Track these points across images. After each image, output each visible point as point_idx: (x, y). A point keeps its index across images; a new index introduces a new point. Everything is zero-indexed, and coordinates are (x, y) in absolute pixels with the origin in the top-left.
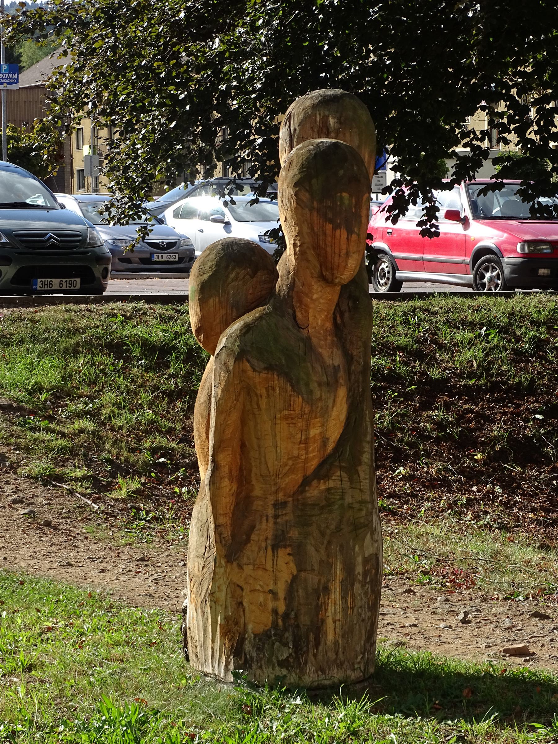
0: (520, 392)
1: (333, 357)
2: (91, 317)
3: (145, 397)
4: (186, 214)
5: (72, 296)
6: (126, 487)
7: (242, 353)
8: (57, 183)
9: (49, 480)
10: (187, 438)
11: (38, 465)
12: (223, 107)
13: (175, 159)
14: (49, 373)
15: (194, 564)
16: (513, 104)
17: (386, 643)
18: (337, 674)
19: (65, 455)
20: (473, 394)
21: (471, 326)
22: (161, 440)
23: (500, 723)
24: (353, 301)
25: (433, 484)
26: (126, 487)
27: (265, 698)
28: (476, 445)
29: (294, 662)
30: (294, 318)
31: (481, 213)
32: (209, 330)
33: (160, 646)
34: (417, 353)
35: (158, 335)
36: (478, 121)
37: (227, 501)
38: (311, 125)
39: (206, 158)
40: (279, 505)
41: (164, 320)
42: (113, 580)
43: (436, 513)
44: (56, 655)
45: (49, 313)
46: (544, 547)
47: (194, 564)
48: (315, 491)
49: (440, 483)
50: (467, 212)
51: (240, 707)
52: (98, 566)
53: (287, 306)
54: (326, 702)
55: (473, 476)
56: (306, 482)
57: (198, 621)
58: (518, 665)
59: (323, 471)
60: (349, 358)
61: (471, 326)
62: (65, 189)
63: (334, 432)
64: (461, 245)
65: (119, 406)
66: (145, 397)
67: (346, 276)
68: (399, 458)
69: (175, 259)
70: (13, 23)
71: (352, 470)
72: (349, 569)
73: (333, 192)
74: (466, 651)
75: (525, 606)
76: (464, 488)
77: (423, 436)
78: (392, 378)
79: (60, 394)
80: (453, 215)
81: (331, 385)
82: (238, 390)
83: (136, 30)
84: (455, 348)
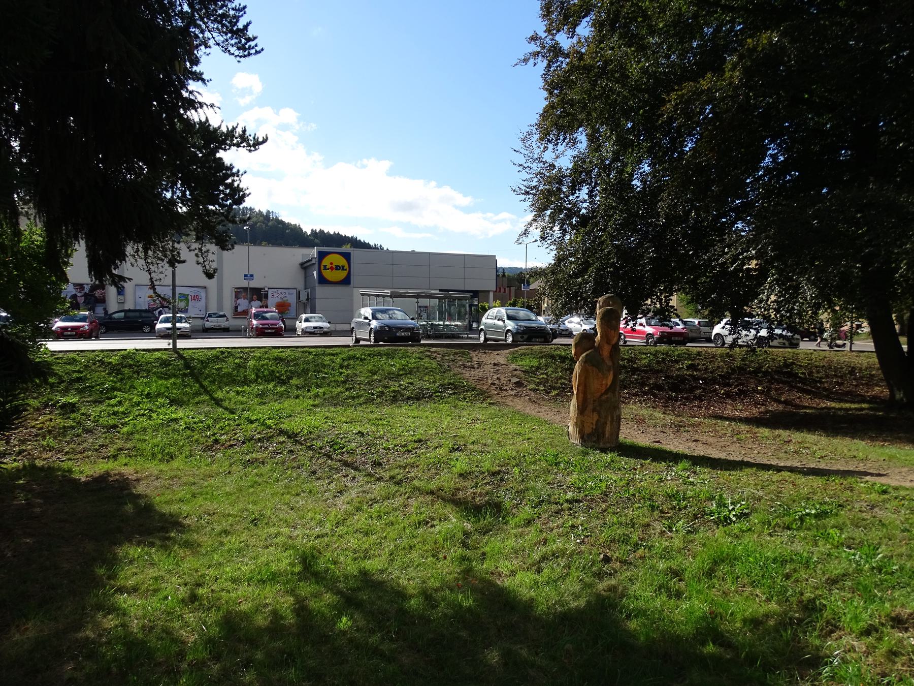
0: (658, 371)
1: (609, 363)
2: (546, 349)
3: (559, 370)
4: (571, 322)
5: (541, 343)
6: (554, 393)
7: (586, 361)
8: (539, 314)
9: (534, 390)
10: (570, 380)
11: (532, 386)
12: (581, 296)
13: (569, 309)
14: (535, 363)
15: (571, 415)
16: (657, 297)
17: (621, 437)
18: (608, 445)
19: (539, 384)
20: (646, 372)
21: (646, 354)
22: (563, 381)
23: (652, 461)
24: (615, 348)
25: (634, 395)
26: (554, 393)
27: (590, 451)
28: (646, 385)
29: (598, 441)
30: (599, 352)
31: (649, 324)
32: (577, 355)
33: (562, 435)
34: (631, 360)
35: (563, 354)
36: (649, 302)
37: (581, 399)
38: (605, 303)
39: (576, 309)
40: (594, 401)
41: (565, 350)
42: (549, 417)
43: (635, 403)
44: (535, 436)
45: (536, 347)
46: (664, 413)
47: (571, 415)
48: (604, 398)
49: (636, 395)
50: (645, 324)
51: (583, 452)
52: (546, 412)
53: (598, 350)
54: (605, 452)
55: (645, 393)
56: (602, 395)
57: (572, 429)
58: (657, 445)
59: (606, 392)
60: (614, 364)
61: (646, 354)
62: (540, 315)
63: (609, 384)
64: (643, 332)
65: (552, 372)
66: (559, 370)
67: (614, 342)
68: (625, 388)
69: (569, 334)
70: (772, 597)
71: (614, 393)
72: (612, 418)
73: (610, 320)
74: (643, 441)
75: (659, 429)
76: (643, 396)
77: (632, 382)
78: (624, 367)
79: (538, 368)
80: (641, 325)
81: (609, 370)
82: (584, 371)
83: (560, 276)
84: (641, 359)
